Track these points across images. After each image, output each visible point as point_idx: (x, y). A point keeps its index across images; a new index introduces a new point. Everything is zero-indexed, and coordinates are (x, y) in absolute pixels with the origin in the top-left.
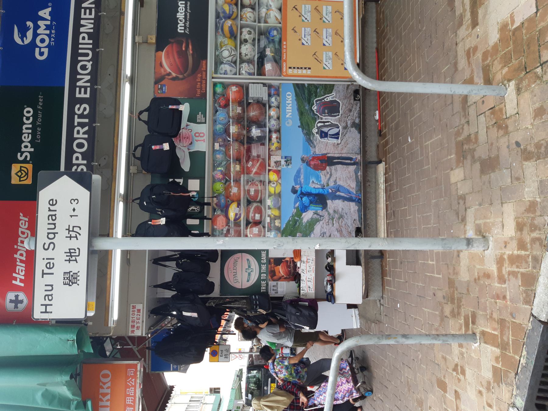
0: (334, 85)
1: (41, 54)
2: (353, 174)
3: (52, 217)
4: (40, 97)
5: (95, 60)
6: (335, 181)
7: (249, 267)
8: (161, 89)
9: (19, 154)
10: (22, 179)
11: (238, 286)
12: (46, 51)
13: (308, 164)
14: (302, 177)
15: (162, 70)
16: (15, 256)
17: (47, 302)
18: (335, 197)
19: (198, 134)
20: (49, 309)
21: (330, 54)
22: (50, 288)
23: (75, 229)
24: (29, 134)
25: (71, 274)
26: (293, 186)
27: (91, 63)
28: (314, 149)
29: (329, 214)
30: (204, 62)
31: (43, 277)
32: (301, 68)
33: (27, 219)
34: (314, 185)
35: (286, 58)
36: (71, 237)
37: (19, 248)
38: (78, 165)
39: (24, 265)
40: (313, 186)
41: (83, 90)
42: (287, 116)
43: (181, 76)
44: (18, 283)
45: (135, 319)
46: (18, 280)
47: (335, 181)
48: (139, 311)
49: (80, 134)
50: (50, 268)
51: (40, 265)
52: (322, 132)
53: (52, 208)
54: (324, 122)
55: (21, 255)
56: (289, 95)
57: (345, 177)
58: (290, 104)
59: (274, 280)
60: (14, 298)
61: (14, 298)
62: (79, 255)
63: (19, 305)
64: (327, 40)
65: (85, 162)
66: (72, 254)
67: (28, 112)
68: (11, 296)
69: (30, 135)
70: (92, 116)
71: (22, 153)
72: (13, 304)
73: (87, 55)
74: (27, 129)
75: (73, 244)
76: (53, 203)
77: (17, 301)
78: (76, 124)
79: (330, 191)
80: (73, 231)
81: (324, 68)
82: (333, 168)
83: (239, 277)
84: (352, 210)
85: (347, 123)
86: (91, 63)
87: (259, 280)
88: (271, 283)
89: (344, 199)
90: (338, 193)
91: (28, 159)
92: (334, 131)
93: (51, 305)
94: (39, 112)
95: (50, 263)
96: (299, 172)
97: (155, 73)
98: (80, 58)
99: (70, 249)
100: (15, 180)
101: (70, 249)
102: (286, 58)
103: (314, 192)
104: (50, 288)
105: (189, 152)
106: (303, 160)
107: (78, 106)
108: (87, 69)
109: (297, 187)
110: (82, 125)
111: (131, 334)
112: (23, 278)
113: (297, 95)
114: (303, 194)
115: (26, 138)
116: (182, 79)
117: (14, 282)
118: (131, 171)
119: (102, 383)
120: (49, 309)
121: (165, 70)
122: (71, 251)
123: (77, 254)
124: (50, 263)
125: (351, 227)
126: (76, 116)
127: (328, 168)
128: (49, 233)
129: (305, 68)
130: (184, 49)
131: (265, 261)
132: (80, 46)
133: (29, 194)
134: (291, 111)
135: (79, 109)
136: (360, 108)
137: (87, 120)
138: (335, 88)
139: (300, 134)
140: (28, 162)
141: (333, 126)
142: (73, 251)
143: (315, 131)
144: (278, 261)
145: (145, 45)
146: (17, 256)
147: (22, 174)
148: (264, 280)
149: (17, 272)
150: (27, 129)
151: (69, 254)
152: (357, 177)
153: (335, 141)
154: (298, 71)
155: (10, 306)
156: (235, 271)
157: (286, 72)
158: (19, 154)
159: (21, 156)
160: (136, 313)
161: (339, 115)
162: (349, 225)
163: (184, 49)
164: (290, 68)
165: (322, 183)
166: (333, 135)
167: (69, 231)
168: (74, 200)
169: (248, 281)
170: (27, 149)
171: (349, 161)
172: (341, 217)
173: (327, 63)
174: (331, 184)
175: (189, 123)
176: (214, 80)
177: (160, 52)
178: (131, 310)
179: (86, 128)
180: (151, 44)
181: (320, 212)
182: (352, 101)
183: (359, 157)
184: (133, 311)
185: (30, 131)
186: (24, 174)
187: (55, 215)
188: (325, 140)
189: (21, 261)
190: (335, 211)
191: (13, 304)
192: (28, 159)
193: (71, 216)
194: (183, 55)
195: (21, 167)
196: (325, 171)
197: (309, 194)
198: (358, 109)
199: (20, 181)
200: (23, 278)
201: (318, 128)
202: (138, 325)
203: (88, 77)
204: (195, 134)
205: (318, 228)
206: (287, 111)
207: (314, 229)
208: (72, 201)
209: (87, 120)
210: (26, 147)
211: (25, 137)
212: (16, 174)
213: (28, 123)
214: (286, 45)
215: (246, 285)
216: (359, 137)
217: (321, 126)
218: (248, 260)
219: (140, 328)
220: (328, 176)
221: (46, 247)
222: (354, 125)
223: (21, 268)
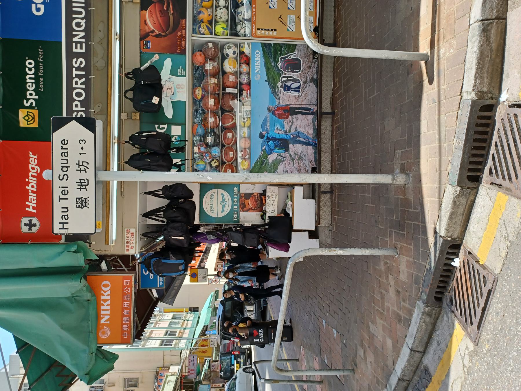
0: (296, 45)
1: (38, 10)
2: (310, 122)
3: (65, 154)
4: (40, 50)
5: (87, 18)
6: (296, 128)
7: (224, 200)
8: (146, 45)
9: (25, 101)
10: (29, 123)
11: (214, 215)
12: (42, 7)
13: (274, 113)
14: (268, 124)
15: (147, 28)
16: (27, 187)
17: (64, 221)
18: (296, 142)
19: (179, 86)
20: (66, 226)
21: (294, 17)
22: (66, 210)
23: (84, 164)
24: (32, 83)
25: (82, 199)
26: (261, 132)
27: (85, 20)
28: (278, 101)
29: (290, 156)
30: (184, 21)
31: (59, 201)
32: (268, 30)
33: (36, 157)
34: (278, 131)
35: (255, 20)
36: (81, 170)
37: (30, 181)
38: (78, 112)
39: (35, 195)
40: (277, 132)
41: (79, 45)
42: (256, 71)
43: (163, 34)
44: (31, 210)
45: (129, 240)
46: (31, 207)
47: (296, 128)
48: (132, 234)
49: (78, 84)
50: (65, 195)
51: (57, 193)
52: (286, 86)
53: (64, 147)
54: (287, 77)
55: (33, 187)
56: (257, 53)
57: (303, 125)
58: (107, 300)
59: (244, 211)
60: (28, 222)
61: (28, 222)
62: (88, 185)
63: (33, 228)
64: (291, 4)
65: (84, 109)
66: (83, 184)
67: (30, 63)
68: (25, 220)
69: (34, 84)
70: (87, 69)
71: (28, 100)
72: (28, 227)
73: (80, 13)
74: (30, 78)
75: (83, 175)
76: (64, 142)
77: (30, 225)
78: (74, 76)
79: (292, 137)
80: (82, 165)
81: (288, 30)
82: (295, 117)
83: (215, 208)
84: (310, 153)
85: (306, 78)
86: (85, 20)
87: (232, 211)
88: (242, 214)
89: (303, 143)
90: (298, 139)
91: (34, 105)
92: (296, 85)
93: (68, 223)
94: (40, 64)
95: (65, 190)
96: (265, 120)
97: (140, 30)
98: (74, 16)
99: (80, 180)
100: (23, 124)
101: (80, 180)
102: (255, 20)
103: (278, 137)
104: (66, 210)
105: (172, 102)
106: (269, 110)
107: (75, 60)
108: (81, 26)
109: (264, 133)
110: (79, 77)
111: (126, 253)
112: (35, 205)
113: (264, 53)
114: (268, 139)
115: (31, 87)
116: (164, 36)
117: (27, 209)
118: (122, 118)
119: (104, 291)
120: (66, 226)
121: (149, 28)
122: (82, 181)
123: (86, 184)
124: (65, 190)
125: (308, 167)
126: (74, 69)
127: (290, 117)
128: (62, 167)
129: (272, 30)
130: (165, 9)
131: (237, 196)
132: (74, 4)
133: (42, 136)
134: (259, 67)
135: (76, 63)
136: (318, 65)
137: (83, 73)
138: (297, 47)
139: (266, 88)
140: (34, 108)
141: (295, 80)
142: (83, 181)
143: (279, 84)
144: (248, 196)
145: (131, 4)
146: (29, 188)
147: (29, 118)
148: (235, 211)
149: (30, 200)
150: (30, 78)
151: (80, 184)
152: (314, 125)
153: (296, 93)
154: (265, 33)
155: (25, 229)
156: (211, 203)
157: (255, 33)
158: (25, 101)
159: (27, 102)
160: (130, 236)
161: (300, 71)
162: (307, 165)
163: (165, 9)
164: (259, 29)
165: (285, 130)
166: (295, 88)
167: (79, 165)
168: (82, 141)
169: (222, 212)
170: (32, 97)
171: (308, 112)
172: (300, 158)
173: (290, 26)
174: (293, 130)
175: (171, 76)
176: (193, 38)
177: (144, 12)
178: (126, 233)
179: (83, 80)
180: (137, 3)
181: (283, 154)
182: (311, 59)
183: (316, 108)
184: (127, 234)
185: (33, 81)
186: (31, 118)
187: (67, 152)
188: (288, 93)
189: (33, 192)
190: (295, 153)
191: (28, 227)
192: (34, 105)
193: (80, 153)
194: (164, 14)
195: (28, 112)
196: (288, 120)
197: (274, 139)
198: (316, 66)
199: (28, 124)
200: (35, 205)
201: (282, 82)
202: (132, 245)
203: (83, 34)
204: (177, 86)
205: (281, 167)
206: (256, 67)
207: (278, 168)
208: (81, 141)
209: (83, 73)
210: (31, 94)
211: (29, 86)
212: (24, 118)
213: (30, 75)
214: (255, 8)
215: (221, 215)
216: (317, 91)
217: (285, 81)
218: (222, 194)
219: (134, 248)
220: (290, 124)
221: (61, 178)
222: (312, 80)
223: (33, 198)
